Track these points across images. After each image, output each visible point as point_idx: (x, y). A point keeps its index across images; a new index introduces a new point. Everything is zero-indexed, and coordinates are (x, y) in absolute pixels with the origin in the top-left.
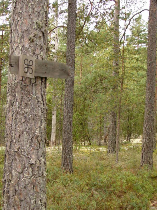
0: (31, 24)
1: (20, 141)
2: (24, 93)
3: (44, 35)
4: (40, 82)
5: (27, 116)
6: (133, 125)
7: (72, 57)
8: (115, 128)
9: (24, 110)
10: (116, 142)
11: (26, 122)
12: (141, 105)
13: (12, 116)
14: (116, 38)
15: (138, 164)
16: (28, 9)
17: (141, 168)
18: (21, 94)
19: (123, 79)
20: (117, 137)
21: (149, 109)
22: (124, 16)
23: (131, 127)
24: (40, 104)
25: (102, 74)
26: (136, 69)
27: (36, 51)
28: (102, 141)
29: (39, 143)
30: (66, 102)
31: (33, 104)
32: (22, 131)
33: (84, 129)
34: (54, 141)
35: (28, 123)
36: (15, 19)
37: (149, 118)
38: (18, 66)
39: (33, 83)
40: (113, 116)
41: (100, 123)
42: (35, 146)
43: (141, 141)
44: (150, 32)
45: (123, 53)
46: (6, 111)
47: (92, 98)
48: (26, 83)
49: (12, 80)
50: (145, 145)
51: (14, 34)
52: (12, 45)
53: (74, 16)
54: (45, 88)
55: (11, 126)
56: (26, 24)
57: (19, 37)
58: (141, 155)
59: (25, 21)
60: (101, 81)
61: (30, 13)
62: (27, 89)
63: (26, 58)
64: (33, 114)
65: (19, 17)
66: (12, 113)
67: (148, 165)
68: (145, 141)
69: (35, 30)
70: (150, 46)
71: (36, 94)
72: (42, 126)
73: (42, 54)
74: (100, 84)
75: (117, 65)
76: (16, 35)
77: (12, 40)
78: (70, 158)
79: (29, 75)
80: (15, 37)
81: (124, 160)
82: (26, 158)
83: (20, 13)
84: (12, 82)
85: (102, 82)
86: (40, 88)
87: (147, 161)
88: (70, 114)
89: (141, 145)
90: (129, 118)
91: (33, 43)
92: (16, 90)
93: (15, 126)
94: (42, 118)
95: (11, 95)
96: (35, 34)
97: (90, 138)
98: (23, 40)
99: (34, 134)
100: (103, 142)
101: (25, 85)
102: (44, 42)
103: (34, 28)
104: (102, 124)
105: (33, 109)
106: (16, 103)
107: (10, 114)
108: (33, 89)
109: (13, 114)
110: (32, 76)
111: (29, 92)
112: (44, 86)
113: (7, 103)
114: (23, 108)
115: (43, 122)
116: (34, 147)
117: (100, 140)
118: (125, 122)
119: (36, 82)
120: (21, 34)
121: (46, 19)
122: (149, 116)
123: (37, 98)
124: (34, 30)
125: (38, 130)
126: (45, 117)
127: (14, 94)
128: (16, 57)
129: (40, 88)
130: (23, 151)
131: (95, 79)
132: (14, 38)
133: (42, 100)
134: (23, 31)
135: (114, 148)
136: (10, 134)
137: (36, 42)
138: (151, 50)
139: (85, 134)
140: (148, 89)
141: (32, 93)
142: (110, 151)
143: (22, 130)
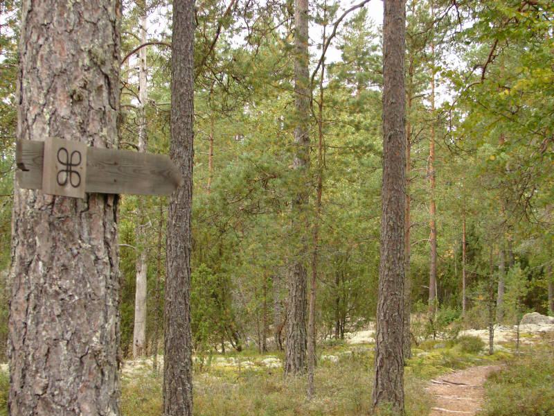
0: (73, 55)
1: (50, 366)
2: (57, 238)
3: (109, 84)
4: (102, 206)
5: (67, 299)
6: (351, 295)
7: (187, 123)
8: (302, 305)
9: (59, 283)
10: (306, 342)
11: (64, 314)
12: (369, 243)
13: (28, 300)
14: (300, 69)
15: (367, 401)
16: (65, 15)
17: (373, 411)
18: (50, 239)
19: (322, 178)
20: (309, 330)
21: (391, 256)
22: (322, 14)
23: (344, 301)
24: (101, 267)
25: (266, 165)
26: (356, 152)
27: (88, 125)
28: (271, 339)
29: (100, 371)
30: (173, 243)
31: (84, 266)
32: (55, 340)
33: (222, 308)
34: (140, 343)
35: (71, 317)
36: (31, 40)
37: (391, 279)
38: (40, 166)
39: (83, 209)
40: (298, 274)
41: (263, 291)
42: (91, 380)
43: (372, 336)
44: (389, 56)
45: (321, 110)
46: (10, 285)
47: (239, 228)
48: (62, 212)
49: (26, 203)
50: (383, 351)
51: (30, 81)
52: (24, 110)
53: (188, 16)
54: (115, 221)
55: (23, 326)
56: (60, 54)
57: (43, 90)
58: (374, 376)
59: (59, 45)
60: (265, 181)
61: (70, 25)
62: (67, 227)
63: (63, 146)
64: (83, 293)
65: (43, 36)
66: (27, 292)
67: (392, 403)
68: (381, 340)
69: (85, 70)
70: (390, 91)
71: (90, 240)
72: (109, 324)
73: (106, 134)
74: (262, 192)
75: (306, 140)
76: (35, 84)
77: (24, 96)
78: (184, 391)
79: (70, 191)
80: (32, 89)
81: (329, 391)
82: (65, 413)
83: (43, 27)
84: (25, 208)
85: (266, 187)
86: (101, 223)
87: (390, 391)
88: (183, 273)
89: (372, 348)
90: (340, 277)
91: (80, 104)
92: (36, 229)
93: (34, 326)
94: (107, 304)
95: (23, 242)
96: (85, 81)
97: (237, 332)
98: (54, 98)
99: (87, 347)
100: (273, 342)
101: (59, 215)
102: (109, 101)
103: (83, 65)
104: (269, 294)
105: (82, 280)
106: (37, 264)
107: (22, 296)
108: (82, 227)
109: (29, 295)
110: (79, 194)
111: (73, 236)
112: (112, 217)
113: (11, 266)
114: (56, 279)
115: (112, 313)
116: (86, 381)
117: (265, 337)
118: (330, 288)
119: (90, 206)
120: (48, 81)
121: (114, 40)
122: (390, 273)
123: (93, 250)
124: (82, 70)
125: (98, 334)
126: (115, 300)
127: (31, 239)
128: (33, 144)
129: (101, 224)
130: (58, 395)
131: (248, 178)
132: (30, 91)
133: (106, 254)
134: (53, 72)
135: (302, 358)
136: (23, 349)
137: (89, 101)
138: (392, 103)
139: (223, 322)
140: (386, 202)
141: (80, 237)
142: (292, 367)
143: (54, 337)
